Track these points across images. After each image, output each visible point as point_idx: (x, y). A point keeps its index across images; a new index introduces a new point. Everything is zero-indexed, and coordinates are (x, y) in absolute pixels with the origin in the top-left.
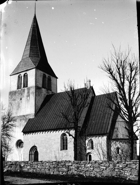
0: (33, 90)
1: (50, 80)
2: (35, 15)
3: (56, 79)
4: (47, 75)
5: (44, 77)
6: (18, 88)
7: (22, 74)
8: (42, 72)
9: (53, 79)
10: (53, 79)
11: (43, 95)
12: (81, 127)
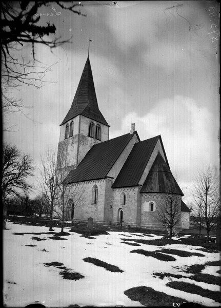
0: (76, 139)
1: (98, 128)
2: (88, 57)
3: (107, 127)
4: (96, 123)
5: (91, 125)
6: (66, 138)
8: (89, 120)
9: (104, 128)
10: (104, 128)
11: (89, 145)
12: (115, 178)
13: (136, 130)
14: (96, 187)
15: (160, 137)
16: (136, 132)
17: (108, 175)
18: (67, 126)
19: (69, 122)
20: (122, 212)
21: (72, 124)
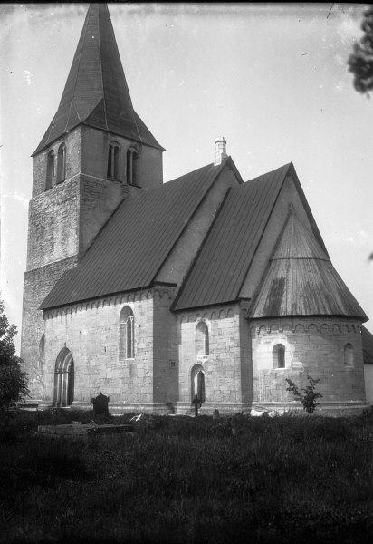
5: (113, 151)
7: (56, 147)
12: (179, 285)
13: (228, 154)
14: (127, 312)
15: (289, 172)
16: (228, 164)
17: (242, 296)
18: (50, 157)
19: (56, 147)
20: (201, 375)
21: (61, 151)
